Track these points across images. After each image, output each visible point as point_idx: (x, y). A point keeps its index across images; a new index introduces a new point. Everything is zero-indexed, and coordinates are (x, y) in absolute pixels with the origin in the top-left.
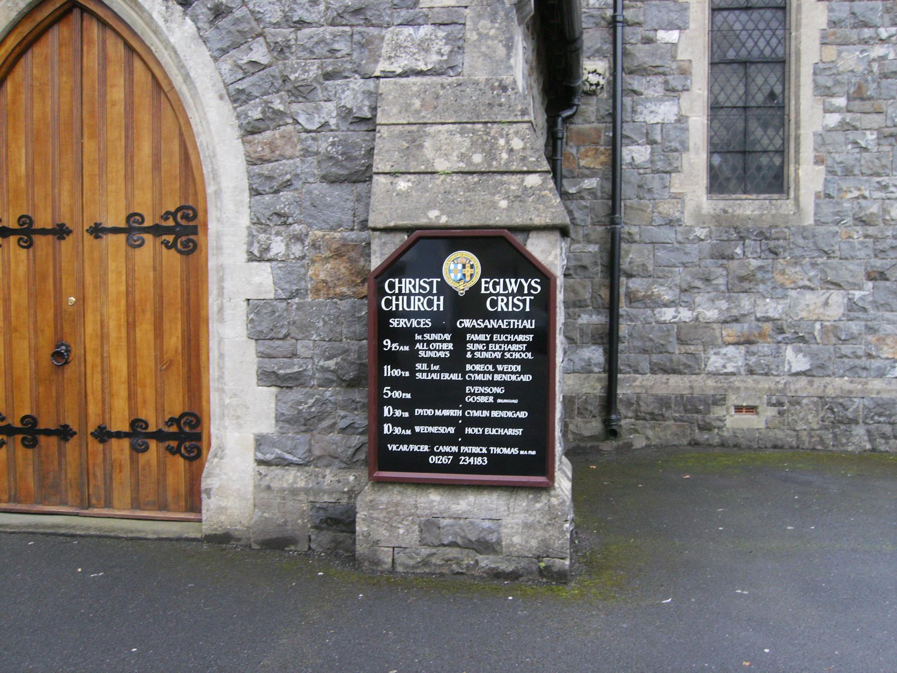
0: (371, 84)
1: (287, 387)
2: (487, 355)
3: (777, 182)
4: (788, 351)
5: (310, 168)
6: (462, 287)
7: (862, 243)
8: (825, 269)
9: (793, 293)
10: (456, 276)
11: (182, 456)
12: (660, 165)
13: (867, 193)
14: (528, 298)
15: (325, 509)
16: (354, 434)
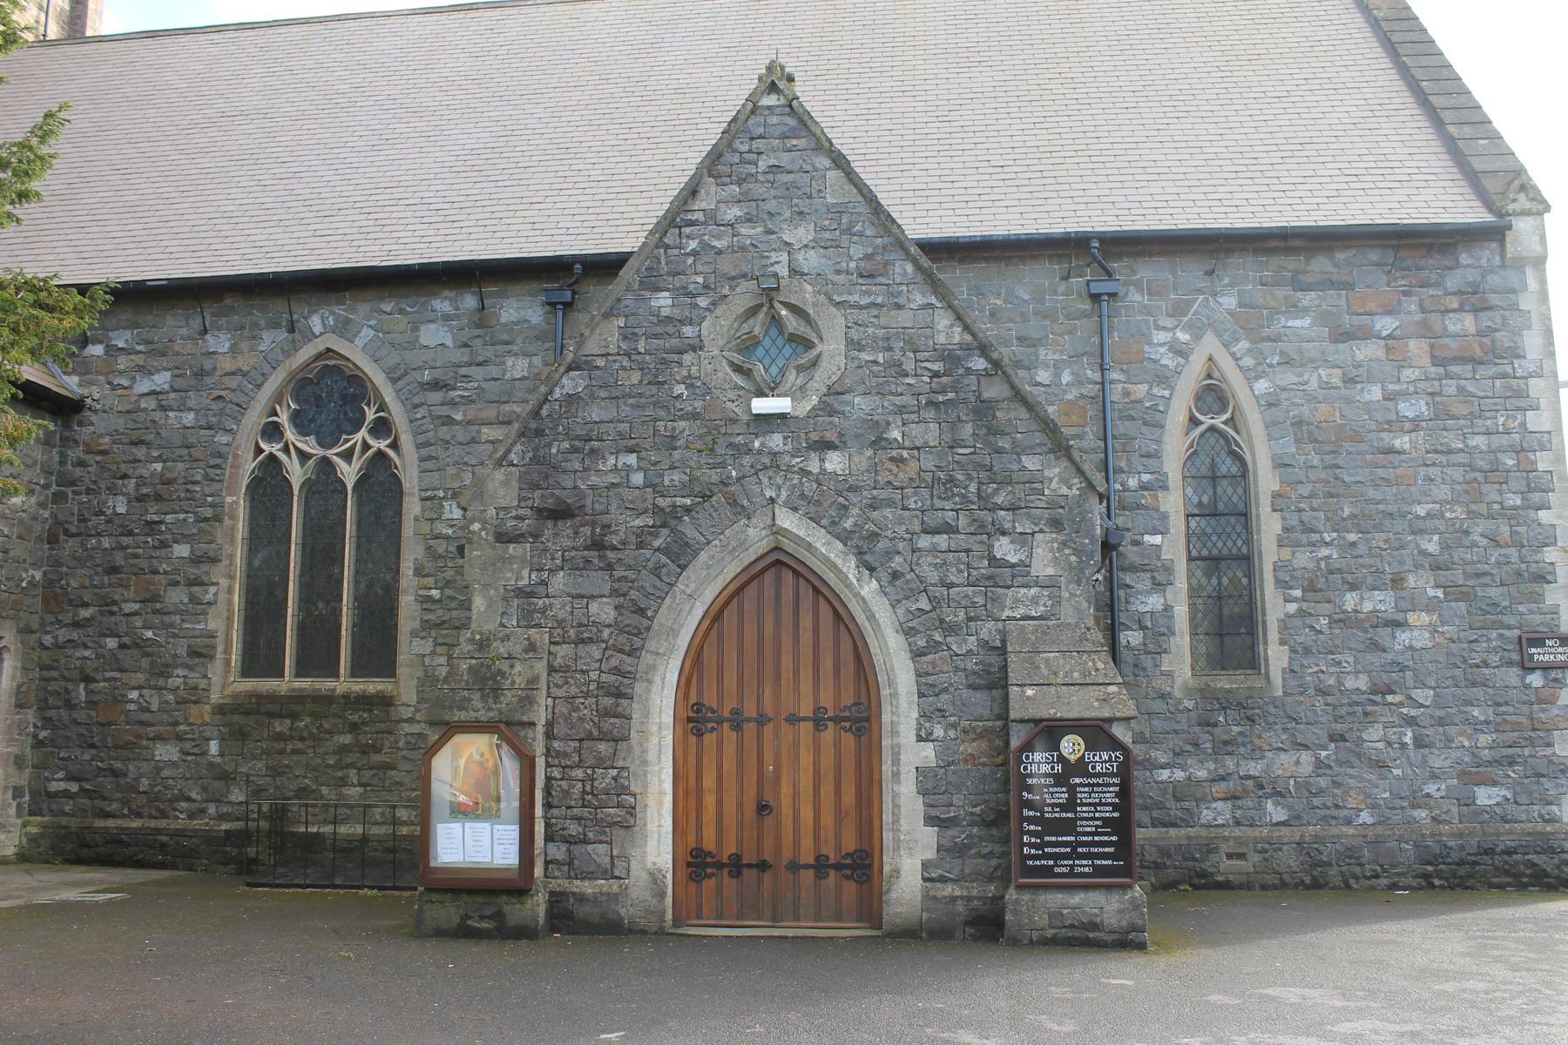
0: (1000, 624)
3: (1251, 661)
5: (959, 679)
9: (1269, 754)
12: (1151, 647)
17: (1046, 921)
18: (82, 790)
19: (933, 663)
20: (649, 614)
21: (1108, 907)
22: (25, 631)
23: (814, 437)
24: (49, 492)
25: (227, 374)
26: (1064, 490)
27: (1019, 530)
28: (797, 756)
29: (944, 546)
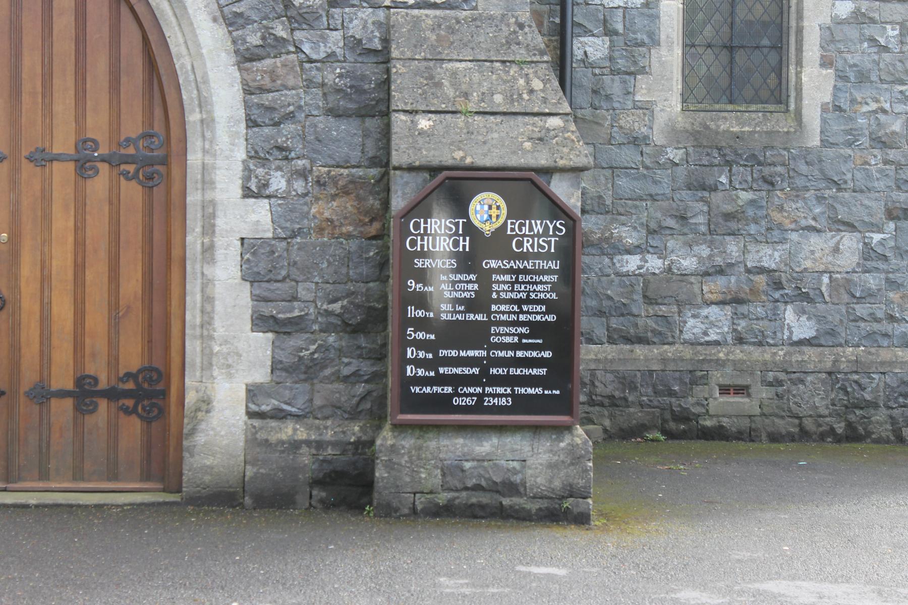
0: (381, 14)
1: (285, 333)
3: (777, 93)
4: (787, 313)
5: (312, 99)
6: (488, 228)
7: (881, 171)
8: (835, 204)
9: (794, 236)
10: (482, 217)
11: (140, 416)
12: (621, 63)
13: (887, 106)
14: (553, 239)
15: (329, 462)
16: (358, 382)
17: (436, 479)
19: (272, 74)
21: (533, 459)
28: (47, 218)
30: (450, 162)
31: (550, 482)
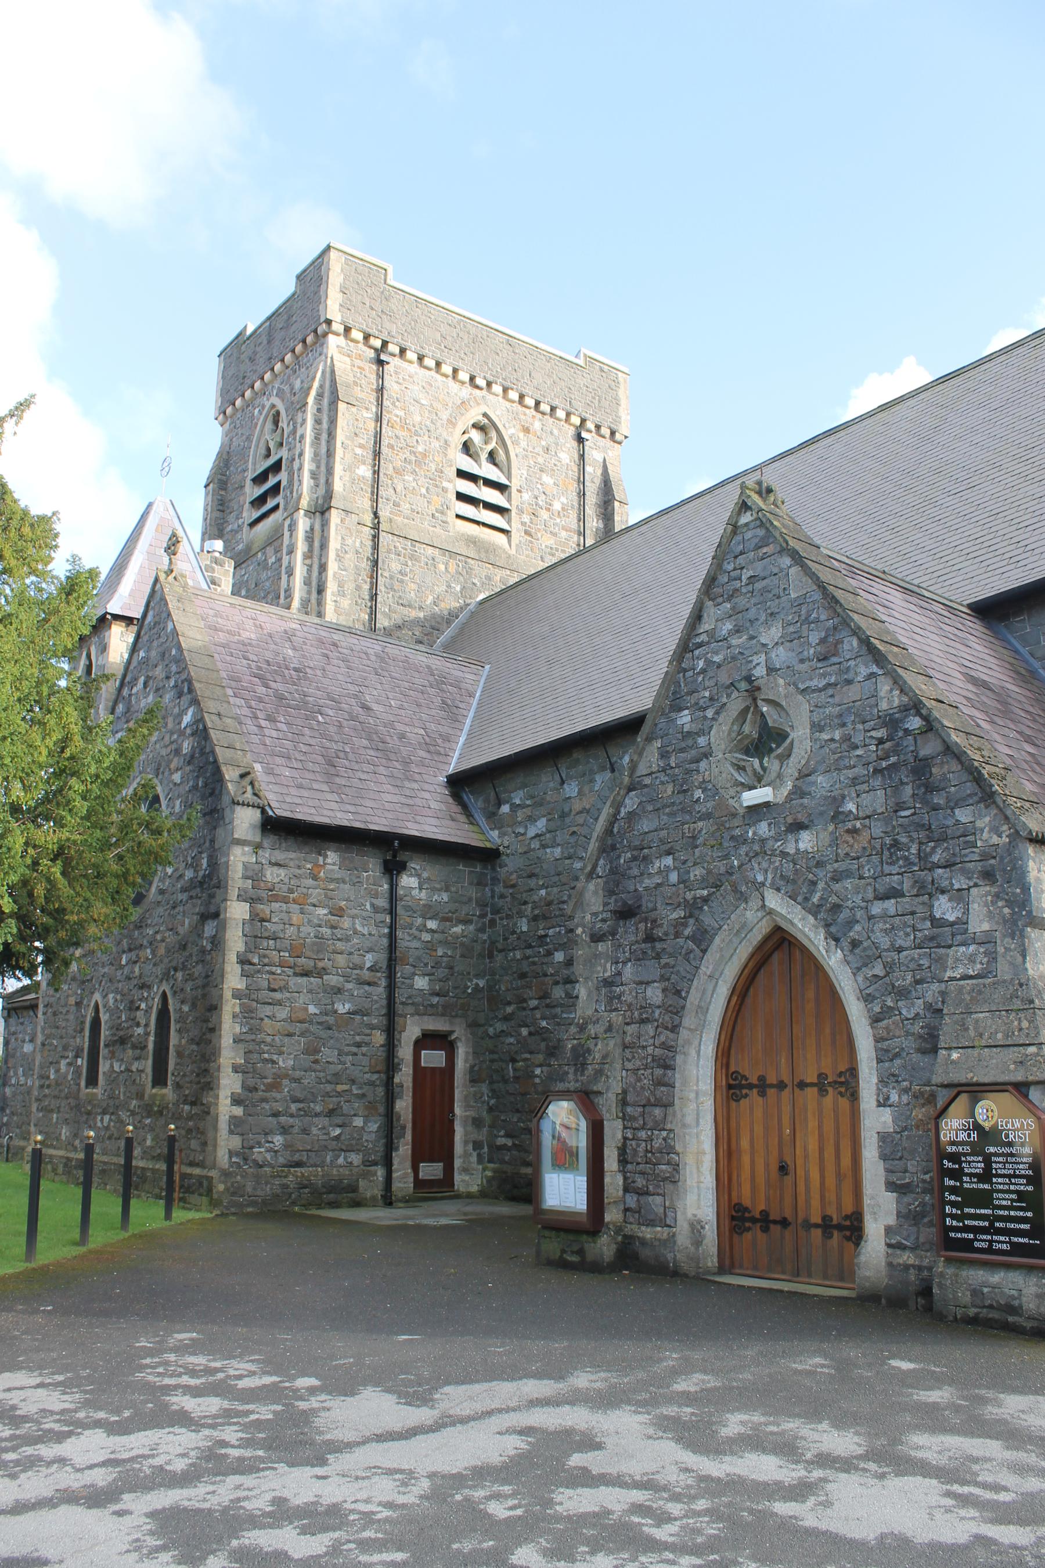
0: (943, 985)
2: (1005, 1172)
18: (514, 1144)
20: (684, 994)
22: (473, 1025)
23: (790, 820)
24: (487, 920)
25: (578, 813)
26: (995, 840)
27: (956, 887)
29: (892, 911)
30: (964, 1081)
31: (1038, 1307)
